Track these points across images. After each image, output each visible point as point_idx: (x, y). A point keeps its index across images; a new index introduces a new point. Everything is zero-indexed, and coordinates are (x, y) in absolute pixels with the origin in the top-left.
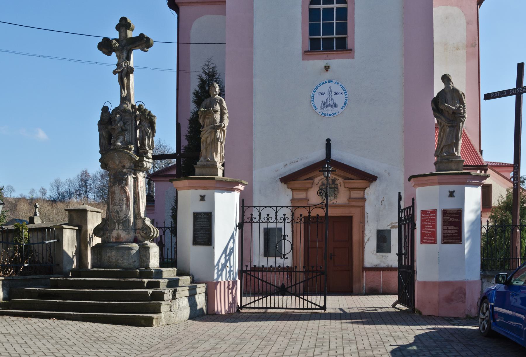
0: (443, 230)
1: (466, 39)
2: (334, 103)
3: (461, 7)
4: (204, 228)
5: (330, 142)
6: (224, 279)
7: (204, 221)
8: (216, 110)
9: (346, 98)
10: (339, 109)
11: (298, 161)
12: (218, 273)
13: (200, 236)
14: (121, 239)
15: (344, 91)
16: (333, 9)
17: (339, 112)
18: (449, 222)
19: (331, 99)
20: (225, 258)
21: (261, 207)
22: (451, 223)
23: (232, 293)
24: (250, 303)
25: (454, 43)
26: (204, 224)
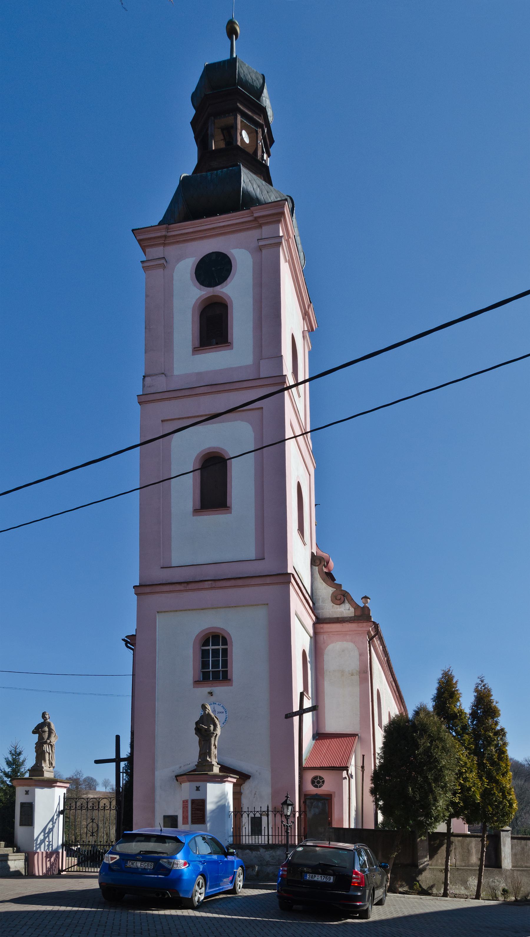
0: (192, 814)
1: (359, 667)
3: (354, 642)
6: (42, 850)
8: (43, 731)
9: (227, 716)
11: (190, 764)
12: (36, 846)
16: (219, 649)
18: (196, 809)
20: (44, 835)
23: (50, 860)
25: (349, 671)
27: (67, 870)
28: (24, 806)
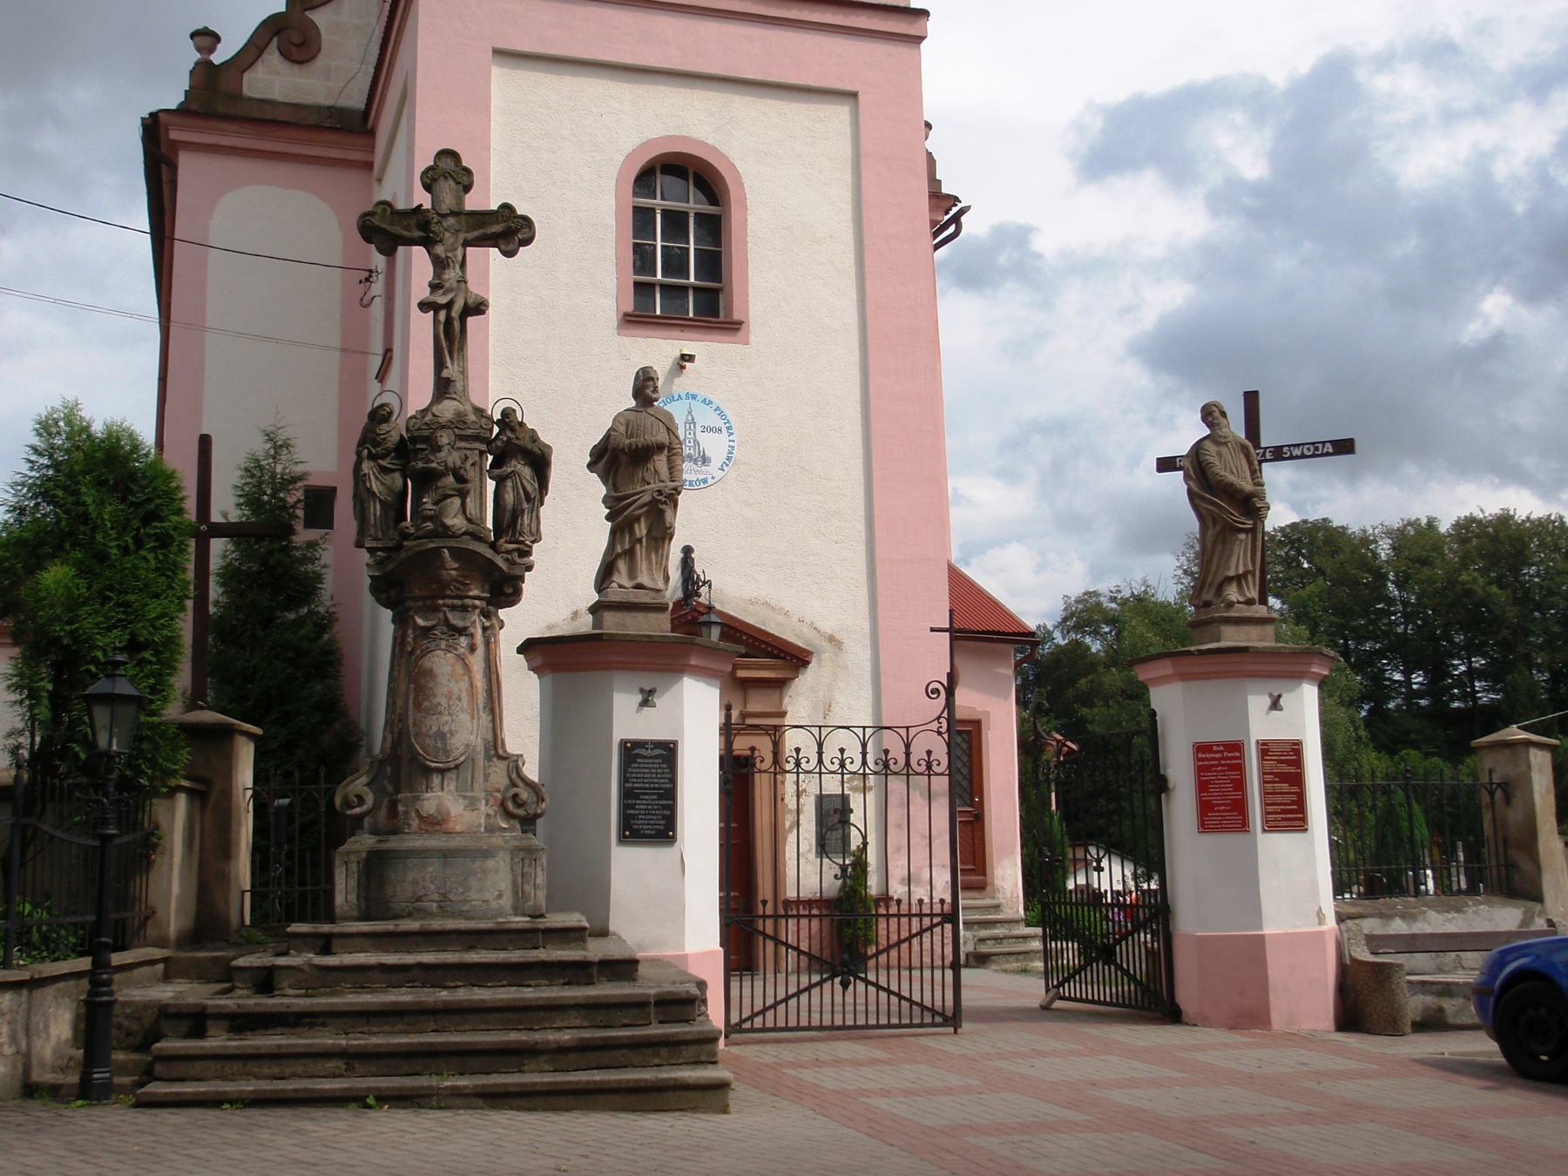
0: (1265, 794)
4: (653, 789)
8: (462, 476)
9: (731, 444)
10: (713, 469)
13: (643, 812)
14: (451, 825)
17: (713, 478)
22: (1283, 778)
24: (751, 1018)
26: (654, 776)
27: (747, 1025)
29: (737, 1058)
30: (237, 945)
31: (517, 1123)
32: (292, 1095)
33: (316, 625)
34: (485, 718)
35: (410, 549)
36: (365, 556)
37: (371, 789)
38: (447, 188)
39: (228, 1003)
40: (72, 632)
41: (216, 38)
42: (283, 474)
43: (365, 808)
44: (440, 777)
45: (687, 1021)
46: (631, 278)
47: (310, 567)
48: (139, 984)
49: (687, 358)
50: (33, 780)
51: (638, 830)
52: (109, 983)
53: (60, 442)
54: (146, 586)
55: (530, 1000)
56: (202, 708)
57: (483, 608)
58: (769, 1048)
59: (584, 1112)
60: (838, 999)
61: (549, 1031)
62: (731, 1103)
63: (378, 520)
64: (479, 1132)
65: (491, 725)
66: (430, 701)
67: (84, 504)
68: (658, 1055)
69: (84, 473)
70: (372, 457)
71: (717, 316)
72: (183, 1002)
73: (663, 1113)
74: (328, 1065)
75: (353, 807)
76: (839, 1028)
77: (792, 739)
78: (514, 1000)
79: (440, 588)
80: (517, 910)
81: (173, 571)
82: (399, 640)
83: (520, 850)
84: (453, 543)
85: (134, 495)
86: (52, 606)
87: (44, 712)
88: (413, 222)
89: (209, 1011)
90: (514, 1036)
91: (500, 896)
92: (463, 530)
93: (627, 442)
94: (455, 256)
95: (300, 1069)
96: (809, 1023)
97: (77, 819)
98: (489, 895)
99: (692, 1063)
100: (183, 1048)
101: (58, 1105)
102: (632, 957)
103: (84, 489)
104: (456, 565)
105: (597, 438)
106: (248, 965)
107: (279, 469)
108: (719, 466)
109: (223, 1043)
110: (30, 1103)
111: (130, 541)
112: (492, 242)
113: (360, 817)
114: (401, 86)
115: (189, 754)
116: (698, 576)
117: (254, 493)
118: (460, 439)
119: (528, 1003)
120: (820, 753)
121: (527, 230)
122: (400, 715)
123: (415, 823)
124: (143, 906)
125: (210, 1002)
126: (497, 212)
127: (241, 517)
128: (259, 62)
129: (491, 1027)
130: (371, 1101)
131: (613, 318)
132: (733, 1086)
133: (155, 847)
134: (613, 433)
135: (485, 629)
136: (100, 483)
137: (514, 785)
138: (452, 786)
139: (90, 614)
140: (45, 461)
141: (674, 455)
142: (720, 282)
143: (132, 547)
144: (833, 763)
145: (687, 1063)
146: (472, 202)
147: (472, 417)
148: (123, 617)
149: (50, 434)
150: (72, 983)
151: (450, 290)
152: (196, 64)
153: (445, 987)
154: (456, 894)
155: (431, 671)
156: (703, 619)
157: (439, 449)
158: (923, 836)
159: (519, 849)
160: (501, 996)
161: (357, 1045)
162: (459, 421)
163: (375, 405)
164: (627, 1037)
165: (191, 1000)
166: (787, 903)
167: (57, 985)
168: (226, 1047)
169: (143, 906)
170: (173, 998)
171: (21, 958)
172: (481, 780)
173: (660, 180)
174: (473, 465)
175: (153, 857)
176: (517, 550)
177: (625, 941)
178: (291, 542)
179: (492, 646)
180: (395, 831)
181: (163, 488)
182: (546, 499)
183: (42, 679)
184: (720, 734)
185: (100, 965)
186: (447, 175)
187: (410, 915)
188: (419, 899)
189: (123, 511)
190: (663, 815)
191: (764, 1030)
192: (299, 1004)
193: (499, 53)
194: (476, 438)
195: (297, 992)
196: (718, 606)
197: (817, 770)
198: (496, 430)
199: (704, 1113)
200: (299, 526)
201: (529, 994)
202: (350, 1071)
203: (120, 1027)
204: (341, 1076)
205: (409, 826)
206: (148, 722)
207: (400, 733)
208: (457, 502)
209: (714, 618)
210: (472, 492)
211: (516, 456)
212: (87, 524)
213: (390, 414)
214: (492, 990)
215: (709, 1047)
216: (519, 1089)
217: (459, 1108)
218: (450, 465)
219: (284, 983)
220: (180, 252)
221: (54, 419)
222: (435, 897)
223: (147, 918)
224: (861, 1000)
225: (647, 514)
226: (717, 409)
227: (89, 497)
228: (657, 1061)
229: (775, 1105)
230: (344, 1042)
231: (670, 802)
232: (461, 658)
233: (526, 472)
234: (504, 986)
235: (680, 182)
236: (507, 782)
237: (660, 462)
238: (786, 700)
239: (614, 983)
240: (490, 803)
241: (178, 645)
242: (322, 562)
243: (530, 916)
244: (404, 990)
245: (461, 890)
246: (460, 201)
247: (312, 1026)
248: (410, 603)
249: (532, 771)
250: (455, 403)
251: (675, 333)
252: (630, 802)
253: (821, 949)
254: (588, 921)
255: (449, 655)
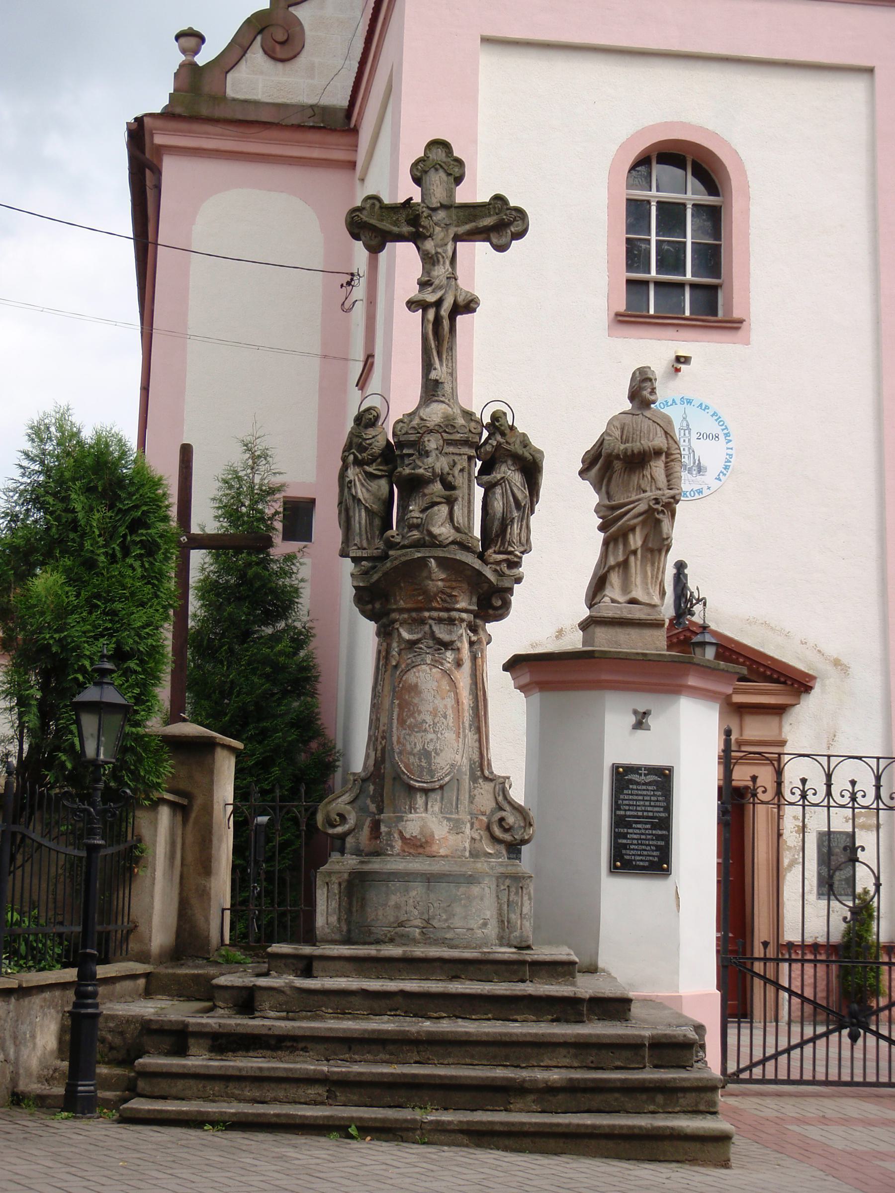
2: (697, 462)
5: (686, 571)
7: (649, 793)
9: (730, 452)
10: (709, 479)
13: (635, 842)
14: (435, 848)
15: (723, 430)
17: (709, 488)
19: (689, 449)
21: (880, 760)
26: (647, 803)
27: (745, 1075)
28: (632, 782)
29: (735, 1110)
30: (217, 963)
31: (504, 1164)
32: (274, 1120)
33: (293, 640)
34: (471, 737)
35: (396, 559)
36: (348, 565)
37: (353, 808)
38: (437, 180)
39: (211, 1022)
40: (60, 640)
41: (202, 39)
42: (261, 485)
43: (346, 827)
44: (424, 798)
45: (684, 1067)
46: (623, 275)
47: (287, 581)
48: (121, 998)
49: (682, 360)
50: (22, 788)
51: (630, 861)
52: (94, 995)
53: (51, 448)
54: (133, 594)
55: (516, 1035)
56: (184, 720)
57: (470, 622)
58: (769, 1102)
59: (575, 1157)
60: (846, 1053)
61: (536, 1069)
62: (732, 1157)
63: (363, 529)
64: (465, 1171)
65: (477, 744)
66: (415, 718)
67: (73, 511)
68: (653, 1102)
69: (74, 479)
70: (358, 463)
71: (715, 313)
72: (165, 1019)
73: (659, 1164)
74: (310, 1091)
75: (335, 826)
76: (858, 1084)
77: (793, 772)
78: (500, 1034)
79: (427, 601)
80: (502, 940)
81: (158, 580)
82: (383, 654)
83: (507, 877)
84: (440, 553)
85: (122, 502)
86: (42, 613)
87: (32, 719)
88: (402, 217)
89: (191, 1029)
90: (500, 1073)
91: (485, 925)
92: (450, 539)
93: (622, 447)
94: (445, 251)
95: (281, 1094)
96: (814, 1077)
97: (63, 828)
98: (473, 924)
99: (689, 1112)
100: (164, 1065)
101: (43, 1116)
102: (625, 996)
103: (73, 496)
104: (443, 576)
105: (589, 443)
106: (229, 984)
107: (257, 480)
108: (716, 476)
109: (205, 1063)
110: (16, 1112)
111: (117, 548)
112: (484, 236)
113: (342, 837)
114: (386, 78)
115: (172, 767)
116: (692, 593)
117: (233, 504)
118: (448, 444)
119: (514, 1039)
120: (829, 785)
121: (520, 222)
122: (383, 731)
123: (398, 845)
124: (126, 920)
125: (192, 1020)
126: (489, 204)
127: (218, 529)
128: (243, 62)
129: (476, 1062)
130: (353, 1131)
131: (603, 318)
132: (733, 1140)
133: (137, 860)
134: (607, 438)
135: (471, 643)
136: (89, 490)
137: (501, 809)
138: (436, 808)
139: (78, 622)
140: (37, 467)
141: (672, 460)
142: (719, 277)
143: (119, 555)
144: (843, 796)
145: (684, 1112)
146: (463, 195)
147: (461, 421)
148: (109, 625)
149: (41, 440)
150: (57, 993)
151: (440, 287)
152: (181, 66)
153: (429, 1018)
154: (440, 921)
155: (416, 686)
156: (696, 639)
157: (427, 454)
158: (833, 911)
159: (505, 876)
160: (486, 1030)
161: (338, 1073)
162: (447, 426)
163: (362, 409)
164: (620, 1080)
165: (173, 1017)
166: (790, 946)
167: (44, 995)
168: (208, 1067)
169: (126, 920)
170: (156, 1014)
171: (9, 966)
172: (466, 802)
173: (656, 169)
174: (462, 470)
175: (136, 870)
176: (507, 560)
177: (615, 978)
178: (268, 555)
179: (479, 661)
180: (377, 853)
181: (149, 494)
182: (537, 507)
183: (32, 687)
184: (719, 763)
185: (86, 976)
186: (437, 167)
187: (392, 940)
188: (401, 925)
189: (111, 517)
190: (656, 846)
191: (763, 1081)
192: (280, 1027)
193: (486, 40)
194: (466, 443)
195: (278, 1014)
196: (713, 626)
197: (825, 803)
198: (485, 434)
199: (703, 1166)
200: (277, 539)
201: (516, 1029)
202: (330, 1099)
203: (103, 1041)
204: (322, 1103)
205: (392, 847)
206: (132, 733)
207: (383, 749)
208: (444, 509)
209: (708, 638)
210: (460, 499)
211: (506, 462)
212: (76, 531)
213: (377, 418)
214: (477, 1023)
215: (708, 1096)
216: (506, 1129)
217: (443, 1144)
218: (438, 471)
219: (265, 1003)
220: (164, 258)
221: (45, 424)
222: (418, 922)
223: (129, 932)
224: (871, 1055)
225: (644, 523)
226: (715, 414)
227: (78, 502)
228: (652, 1108)
229: (779, 1162)
230: (325, 1069)
231: (664, 832)
232: (447, 674)
233: (516, 478)
234: (489, 1019)
235: (679, 172)
236: (494, 805)
237: (658, 468)
238: (786, 728)
239: (606, 1023)
240: (475, 827)
241: (162, 655)
242: (300, 576)
243: (516, 947)
244: (386, 1018)
245: (444, 917)
246: (451, 194)
247: (293, 1050)
248: (395, 615)
249: (518, 794)
250: (444, 406)
251: (670, 332)
252: (622, 830)
253: (828, 998)
254: (577, 955)
255: (434, 670)
